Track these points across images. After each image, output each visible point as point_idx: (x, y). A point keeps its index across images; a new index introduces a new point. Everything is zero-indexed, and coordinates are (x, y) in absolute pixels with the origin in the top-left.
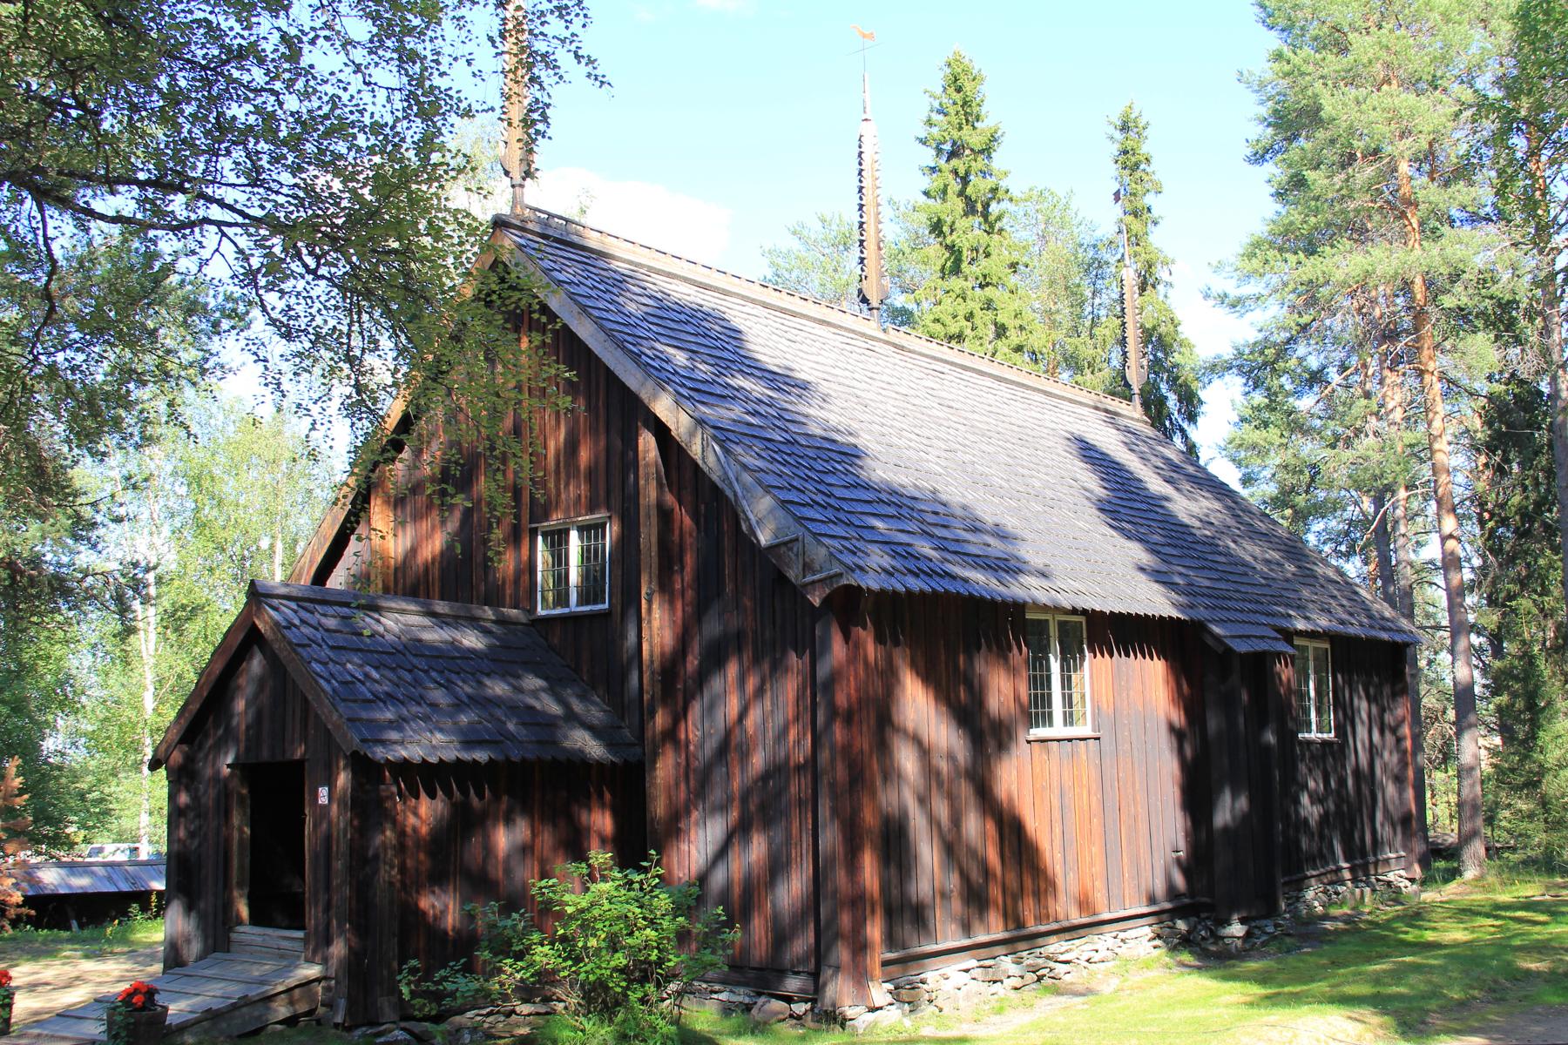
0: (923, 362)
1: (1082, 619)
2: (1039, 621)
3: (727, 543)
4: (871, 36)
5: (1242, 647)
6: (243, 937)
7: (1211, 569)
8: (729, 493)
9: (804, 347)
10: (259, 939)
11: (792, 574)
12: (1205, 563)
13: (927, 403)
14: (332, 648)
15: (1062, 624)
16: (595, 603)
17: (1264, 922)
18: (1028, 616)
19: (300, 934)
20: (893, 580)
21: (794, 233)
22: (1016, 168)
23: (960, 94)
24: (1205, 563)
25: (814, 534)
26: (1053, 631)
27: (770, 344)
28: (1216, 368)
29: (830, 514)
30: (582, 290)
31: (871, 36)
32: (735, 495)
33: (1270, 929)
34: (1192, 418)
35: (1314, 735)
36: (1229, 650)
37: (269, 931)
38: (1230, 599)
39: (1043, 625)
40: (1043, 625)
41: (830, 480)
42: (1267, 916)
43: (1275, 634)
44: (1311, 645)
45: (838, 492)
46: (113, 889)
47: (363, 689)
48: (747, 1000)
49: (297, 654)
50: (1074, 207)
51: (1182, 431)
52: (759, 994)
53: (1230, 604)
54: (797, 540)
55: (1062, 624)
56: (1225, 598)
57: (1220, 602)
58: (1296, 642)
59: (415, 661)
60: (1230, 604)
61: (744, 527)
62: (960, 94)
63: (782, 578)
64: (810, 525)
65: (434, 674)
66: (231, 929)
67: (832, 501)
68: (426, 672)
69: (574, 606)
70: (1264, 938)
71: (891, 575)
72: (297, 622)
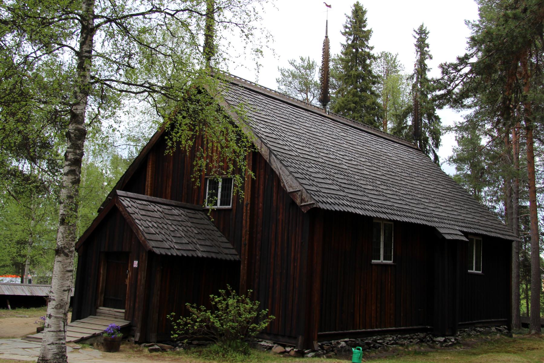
0: (341, 126)
1: (392, 223)
2: (378, 223)
3: (275, 189)
4: (330, 6)
5: (448, 237)
6: (102, 311)
7: (439, 208)
8: (277, 173)
9: (301, 120)
10: (108, 312)
11: (298, 201)
12: (437, 206)
13: (341, 142)
14: (142, 215)
15: (385, 224)
16: (227, 205)
17: (451, 337)
18: (374, 221)
19: (124, 311)
20: (331, 207)
21: (291, 63)
22: (377, 45)
23: (359, 13)
24: (437, 206)
25: (306, 189)
26: (382, 227)
27: (290, 118)
28: (449, 129)
29: (311, 182)
30: (230, 98)
31: (330, 6)
32: (280, 174)
33: (453, 340)
34: (437, 145)
35: (474, 271)
36: (444, 238)
37: (112, 309)
38: (446, 219)
39: (379, 224)
40: (379, 224)
41: (311, 170)
42: (452, 335)
43: (461, 233)
44: (475, 238)
45: (313, 175)
46: (24, 294)
47: (152, 230)
48: (270, 345)
49: (131, 216)
50: (398, 59)
51: (434, 151)
52: (274, 343)
53: (445, 221)
54: (300, 191)
55: (385, 224)
56: (444, 219)
57: (442, 221)
58: (469, 237)
59: (167, 221)
60: (445, 221)
61: (282, 185)
62: (359, 13)
63: (293, 203)
64: (305, 186)
65: (173, 226)
66: (97, 308)
67: (311, 178)
68: (171, 225)
69: (219, 206)
70: (450, 343)
71: (330, 204)
72: (130, 206)
